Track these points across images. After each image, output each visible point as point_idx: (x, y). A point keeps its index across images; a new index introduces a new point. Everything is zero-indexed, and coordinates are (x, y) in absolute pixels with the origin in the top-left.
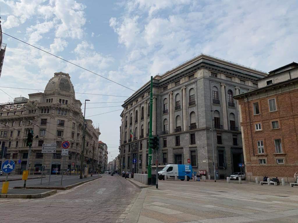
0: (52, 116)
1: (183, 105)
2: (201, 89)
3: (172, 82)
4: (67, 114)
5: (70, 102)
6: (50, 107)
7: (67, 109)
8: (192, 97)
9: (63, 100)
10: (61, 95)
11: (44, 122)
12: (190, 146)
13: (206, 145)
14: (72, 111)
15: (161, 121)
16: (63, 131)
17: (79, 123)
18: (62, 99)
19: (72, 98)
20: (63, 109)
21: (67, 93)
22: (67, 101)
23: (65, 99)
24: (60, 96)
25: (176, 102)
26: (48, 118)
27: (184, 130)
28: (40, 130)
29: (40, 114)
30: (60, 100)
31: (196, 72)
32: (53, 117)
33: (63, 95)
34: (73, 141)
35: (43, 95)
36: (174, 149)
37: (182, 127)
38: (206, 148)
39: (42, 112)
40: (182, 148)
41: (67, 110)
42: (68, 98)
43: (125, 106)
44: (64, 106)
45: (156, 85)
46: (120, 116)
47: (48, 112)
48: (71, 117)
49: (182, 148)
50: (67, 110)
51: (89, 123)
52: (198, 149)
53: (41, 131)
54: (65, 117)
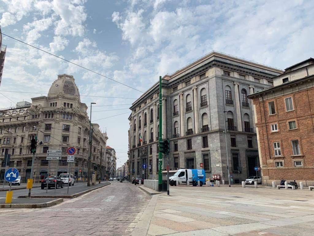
0: (57, 121)
1: (195, 106)
2: (213, 89)
3: (182, 82)
4: (72, 119)
5: (75, 105)
6: (55, 111)
7: (72, 113)
8: (204, 97)
9: (68, 104)
10: (66, 98)
11: (48, 127)
12: (203, 149)
13: (219, 148)
14: (77, 115)
15: (171, 124)
16: (68, 137)
17: (85, 128)
18: (67, 102)
19: (77, 102)
20: (68, 113)
21: (72, 97)
22: (72, 104)
23: (70, 103)
24: (64, 99)
25: (187, 104)
26: (53, 123)
27: (196, 133)
28: (45, 136)
29: (44, 118)
30: (65, 103)
31: (207, 70)
32: (75, 125)
33: (68, 99)
34: (79, 146)
35: (47, 99)
36: (185, 153)
37: (193, 130)
38: (220, 151)
39: (46, 117)
40: (194, 152)
41: (72, 115)
42: (73, 101)
43: (133, 108)
44: (68, 110)
45: (166, 86)
46: (128, 119)
47: (52, 117)
48: (76, 122)
49: (194, 152)
50: (72, 115)
51: (95, 128)
52: (211, 152)
53: (45, 137)
54: (70, 121)
